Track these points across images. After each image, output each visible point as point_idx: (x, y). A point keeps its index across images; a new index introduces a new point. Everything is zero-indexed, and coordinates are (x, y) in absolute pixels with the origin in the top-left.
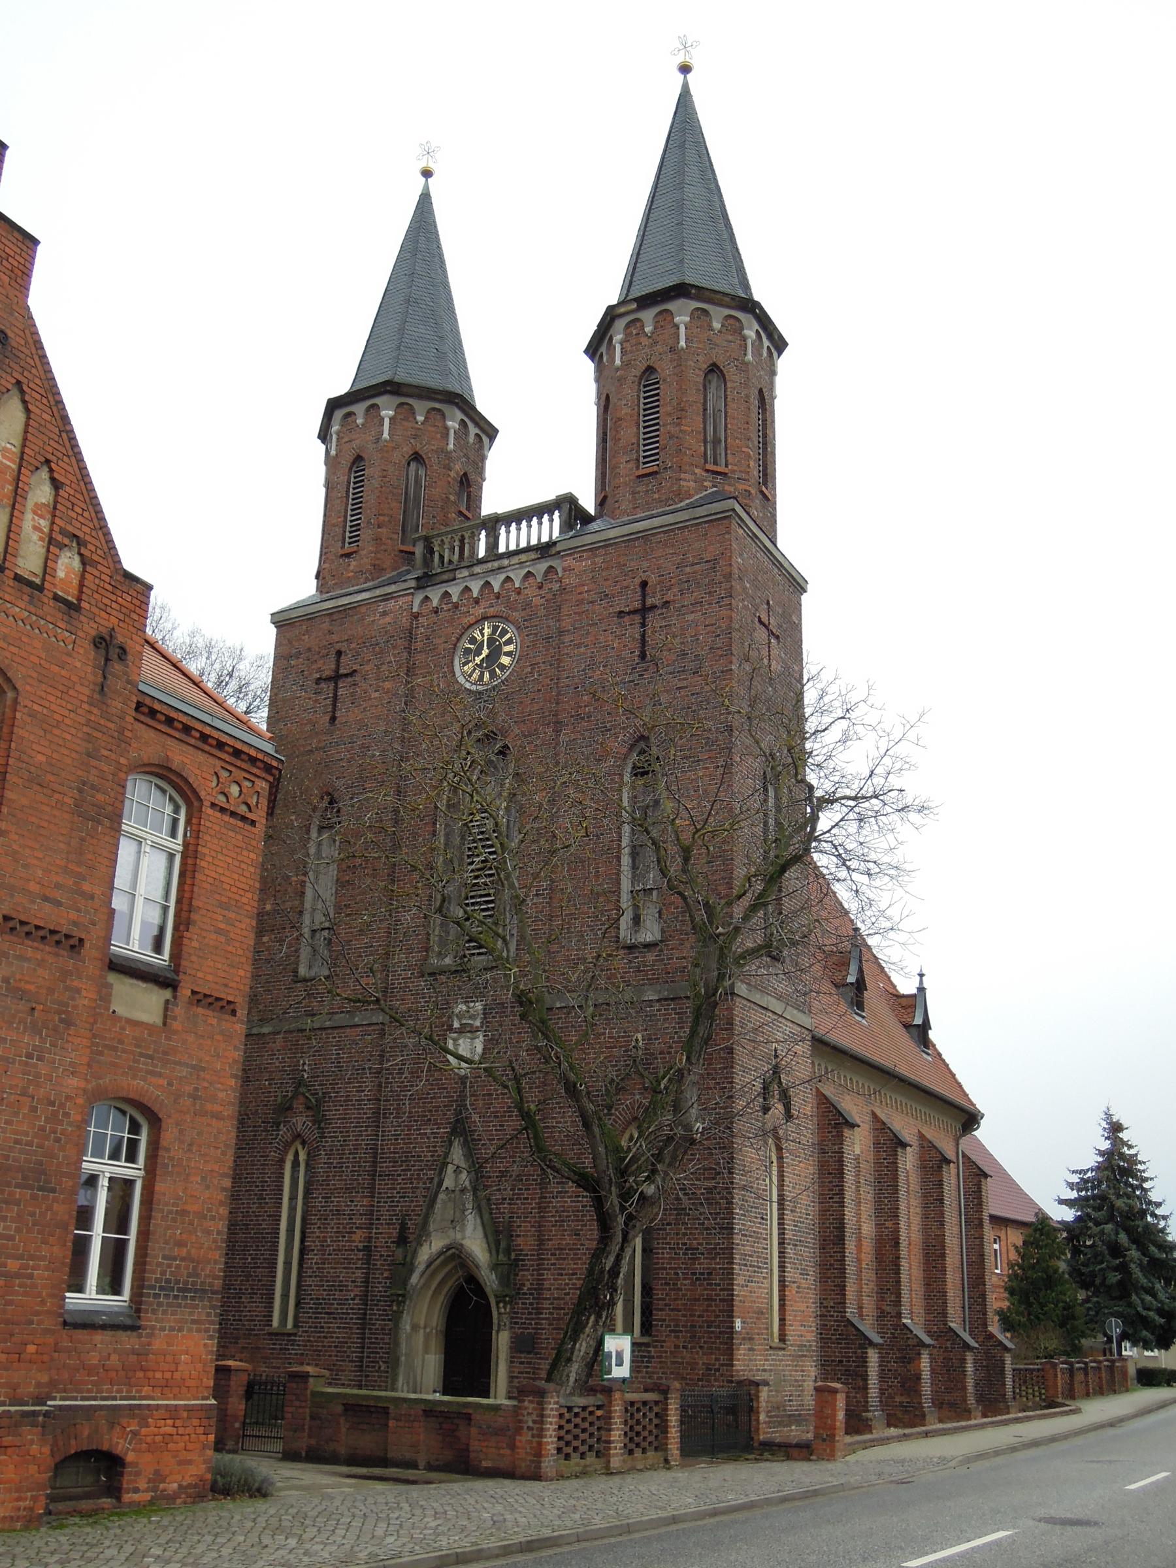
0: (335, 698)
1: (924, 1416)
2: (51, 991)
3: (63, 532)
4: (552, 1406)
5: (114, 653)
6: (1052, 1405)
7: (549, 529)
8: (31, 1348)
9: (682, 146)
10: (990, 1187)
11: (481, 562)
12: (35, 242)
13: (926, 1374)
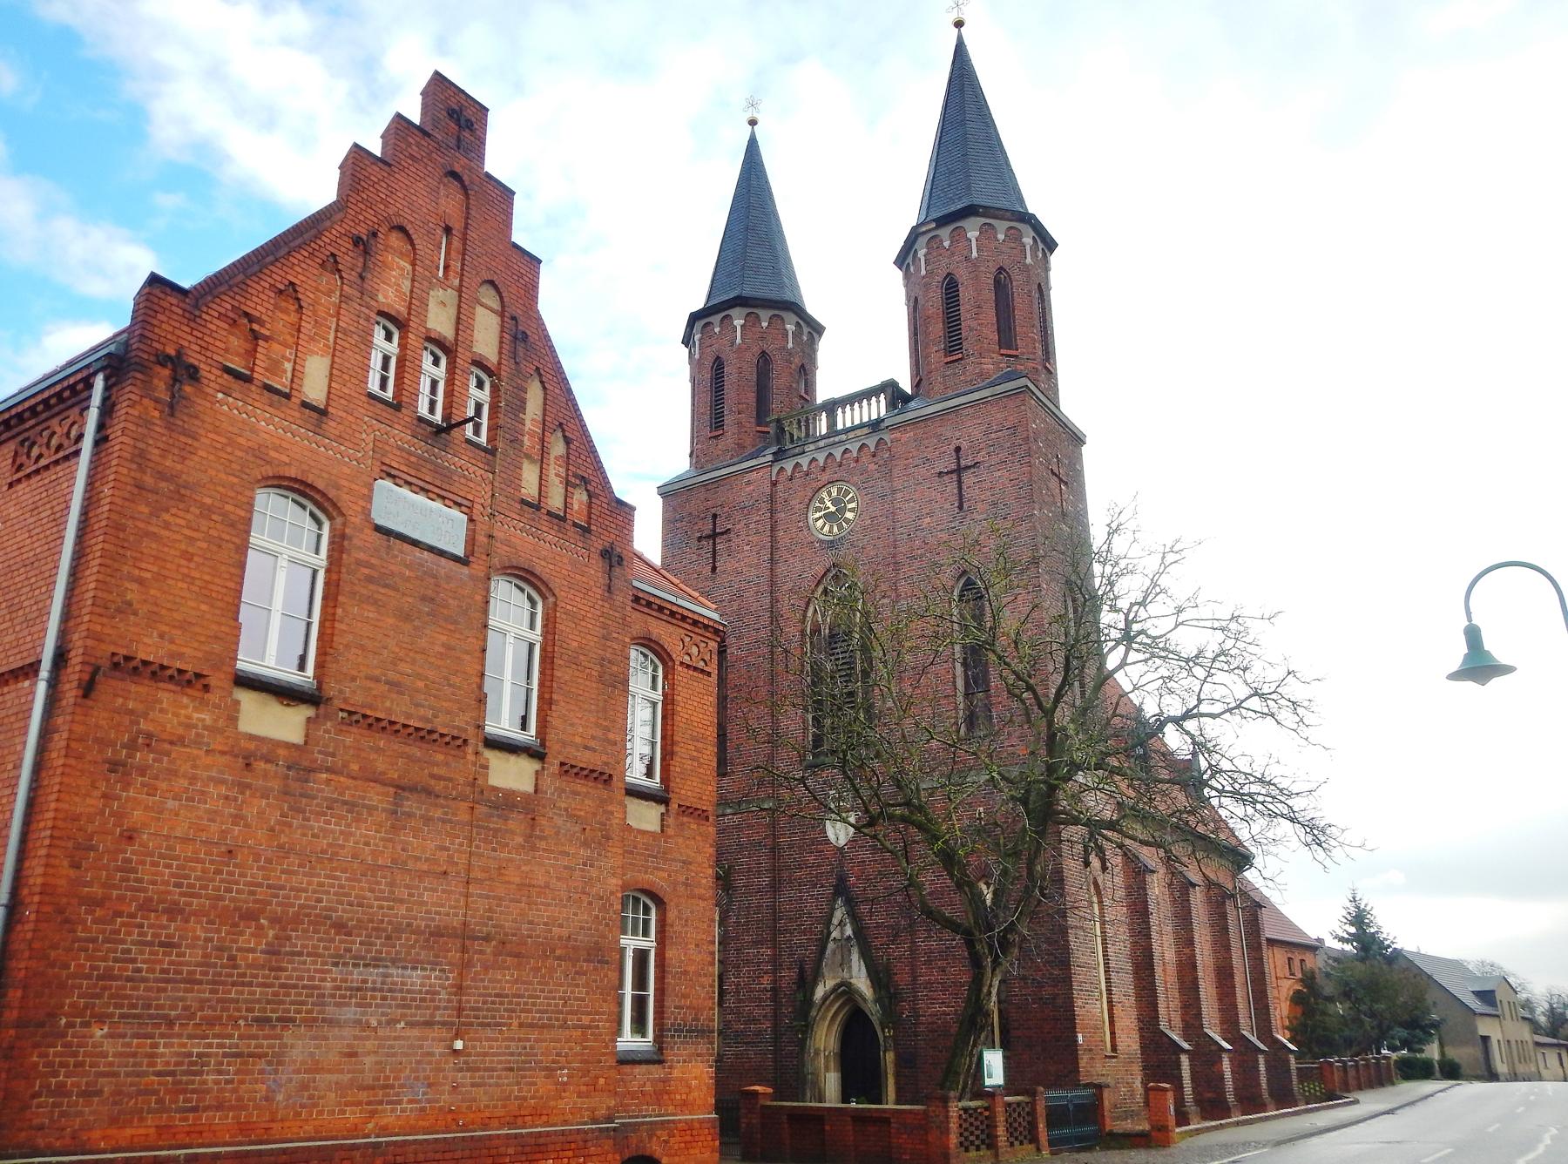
0: (714, 551)
1: (1229, 1109)
2: (595, 814)
3: (575, 475)
4: (954, 1109)
5: (615, 559)
6: (1331, 1096)
7: (877, 408)
8: (602, 1081)
9: (962, 90)
10: (1264, 915)
11: (823, 438)
12: (540, 262)
13: (1228, 1075)
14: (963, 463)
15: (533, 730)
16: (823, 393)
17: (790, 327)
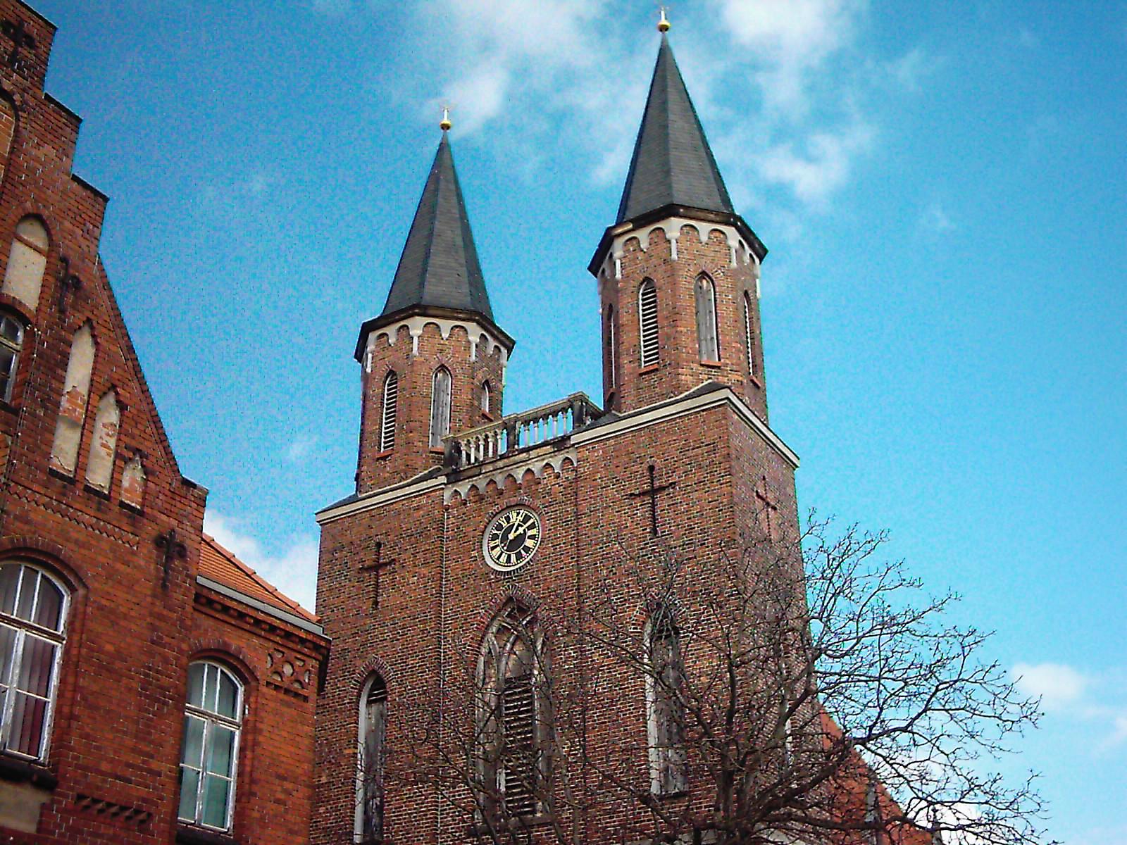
0: (377, 585)
14: (657, 484)
15: (229, 824)
16: (510, 409)
17: (474, 338)
